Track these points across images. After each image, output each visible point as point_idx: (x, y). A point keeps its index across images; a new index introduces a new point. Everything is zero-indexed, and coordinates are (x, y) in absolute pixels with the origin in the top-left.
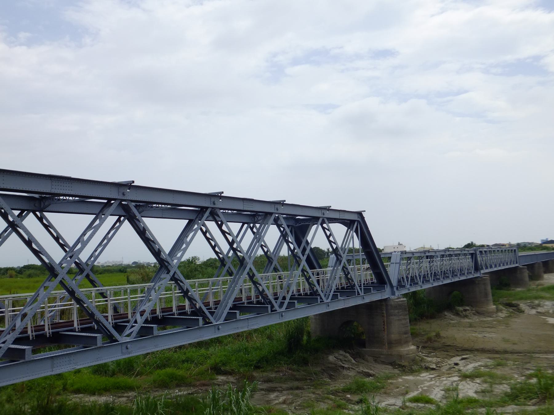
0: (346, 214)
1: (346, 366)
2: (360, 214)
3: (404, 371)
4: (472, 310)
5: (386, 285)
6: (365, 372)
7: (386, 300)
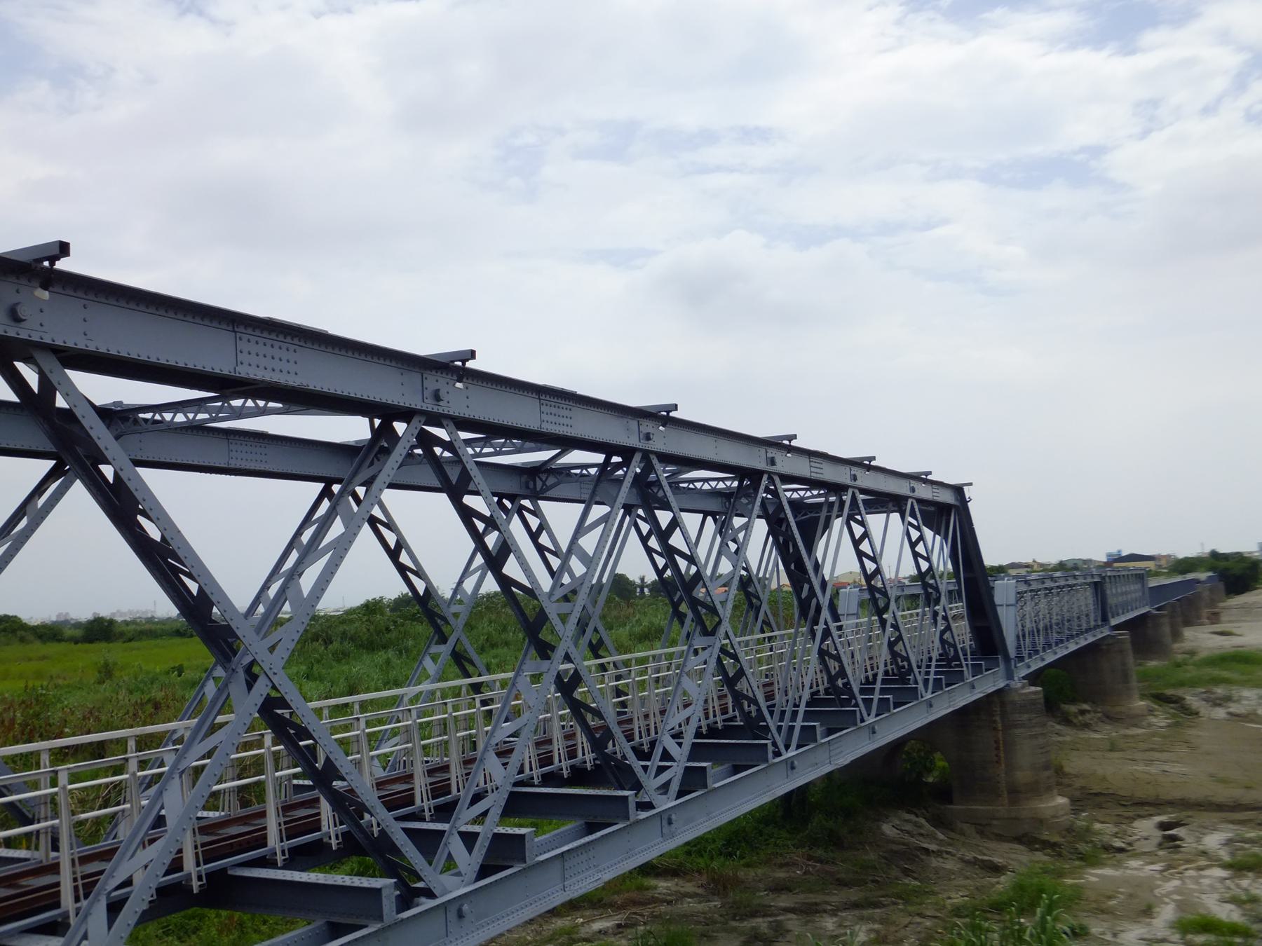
1: (933, 847)
2: (958, 490)
3: (1060, 855)
4: (1095, 712)
6: (983, 861)
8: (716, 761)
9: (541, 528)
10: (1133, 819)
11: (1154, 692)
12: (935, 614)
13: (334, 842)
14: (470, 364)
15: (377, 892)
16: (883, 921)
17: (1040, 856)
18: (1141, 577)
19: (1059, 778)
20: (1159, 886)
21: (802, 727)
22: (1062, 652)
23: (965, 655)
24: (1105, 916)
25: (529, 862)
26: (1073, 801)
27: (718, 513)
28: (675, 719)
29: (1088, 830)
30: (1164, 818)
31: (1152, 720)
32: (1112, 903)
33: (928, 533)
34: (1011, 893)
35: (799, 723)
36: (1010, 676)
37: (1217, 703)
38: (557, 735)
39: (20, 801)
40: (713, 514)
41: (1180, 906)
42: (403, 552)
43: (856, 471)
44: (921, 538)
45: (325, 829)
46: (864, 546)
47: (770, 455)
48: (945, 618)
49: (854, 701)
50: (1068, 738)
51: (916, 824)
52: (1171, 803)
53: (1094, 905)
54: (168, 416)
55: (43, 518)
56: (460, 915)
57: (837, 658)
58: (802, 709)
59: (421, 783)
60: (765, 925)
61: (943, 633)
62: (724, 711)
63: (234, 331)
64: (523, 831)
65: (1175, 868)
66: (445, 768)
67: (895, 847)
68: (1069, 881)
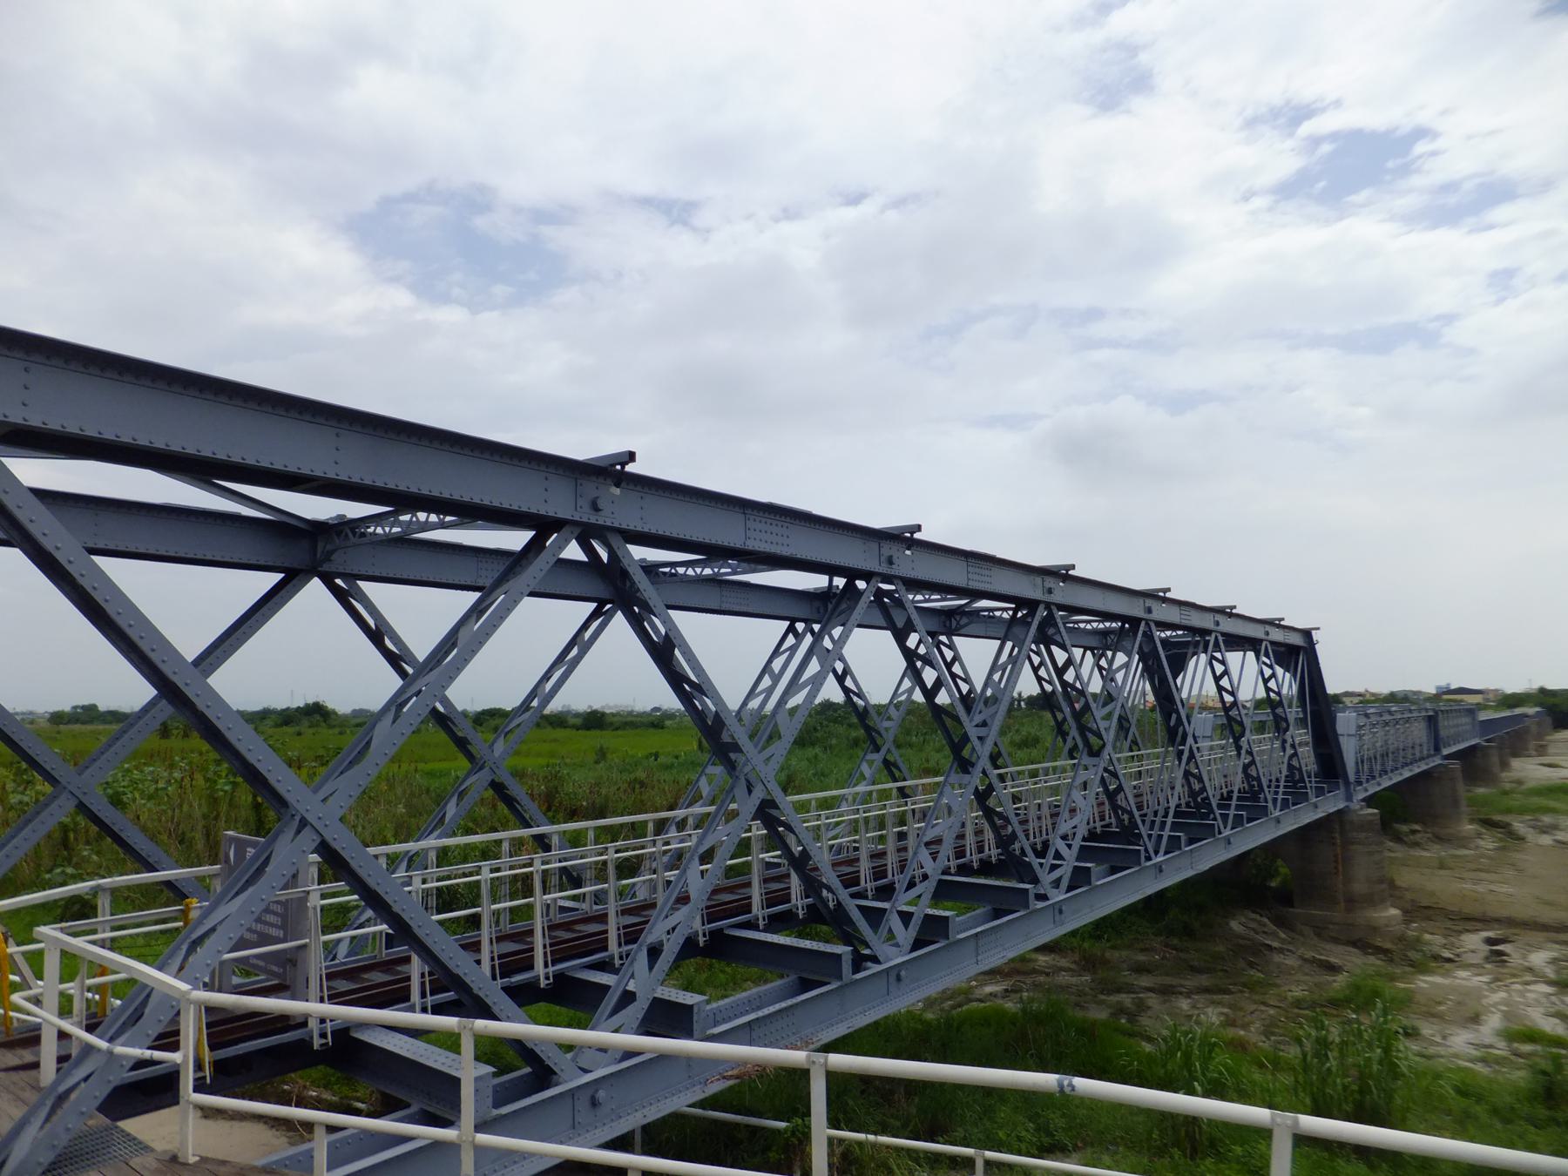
1: (1275, 944)
3: (1391, 960)
6: (1320, 960)
7: (1339, 812)
8: (1098, 862)
9: (955, 659)
10: (1460, 932)
11: (1482, 817)
12: (1284, 741)
13: (801, 913)
14: (916, 536)
15: (838, 957)
16: (1230, 1007)
17: (1372, 959)
18: (1471, 711)
19: (1392, 892)
20: (1486, 997)
21: (1169, 836)
22: (1396, 779)
23: (1309, 777)
24: (1435, 1020)
25: (951, 939)
26: (1405, 912)
27: (1096, 648)
28: (1064, 828)
29: (1418, 940)
30: (1491, 934)
31: (1482, 843)
32: (1442, 1008)
33: (1279, 671)
34: (1347, 992)
35: (1166, 833)
36: (1349, 798)
37: (1545, 830)
38: (969, 830)
39: (571, 866)
40: (1092, 649)
41: (1507, 1016)
42: (848, 677)
43: (1219, 617)
44: (1274, 675)
45: (794, 901)
46: (1225, 682)
47: (1147, 605)
48: (1293, 746)
49: (1212, 816)
50: (1399, 855)
51: (1260, 923)
52: (1498, 921)
53: (1424, 1009)
54: (681, 570)
55: (589, 648)
56: (899, 979)
57: (1200, 780)
58: (1170, 820)
59: (865, 867)
60: (1129, 1000)
61: (1291, 757)
62: (1102, 819)
63: (744, 513)
64: (947, 913)
65: (1500, 981)
66: (883, 854)
67: (1241, 942)
68: (1403, 985)
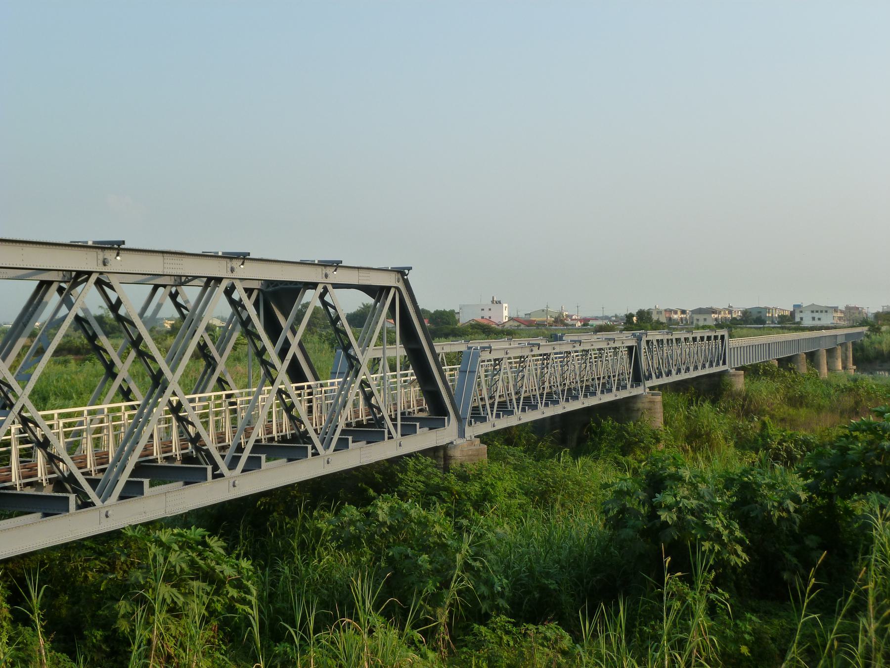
0: (372, 273)
5: (446, 418)
7: (445, 448)
